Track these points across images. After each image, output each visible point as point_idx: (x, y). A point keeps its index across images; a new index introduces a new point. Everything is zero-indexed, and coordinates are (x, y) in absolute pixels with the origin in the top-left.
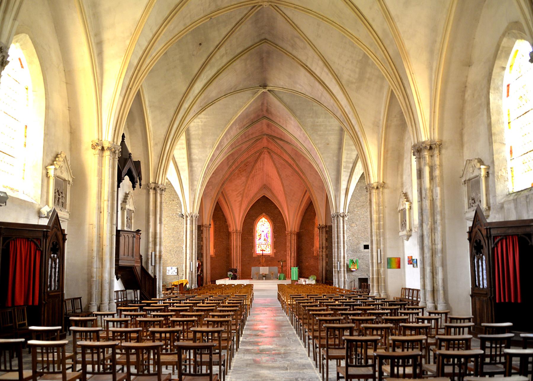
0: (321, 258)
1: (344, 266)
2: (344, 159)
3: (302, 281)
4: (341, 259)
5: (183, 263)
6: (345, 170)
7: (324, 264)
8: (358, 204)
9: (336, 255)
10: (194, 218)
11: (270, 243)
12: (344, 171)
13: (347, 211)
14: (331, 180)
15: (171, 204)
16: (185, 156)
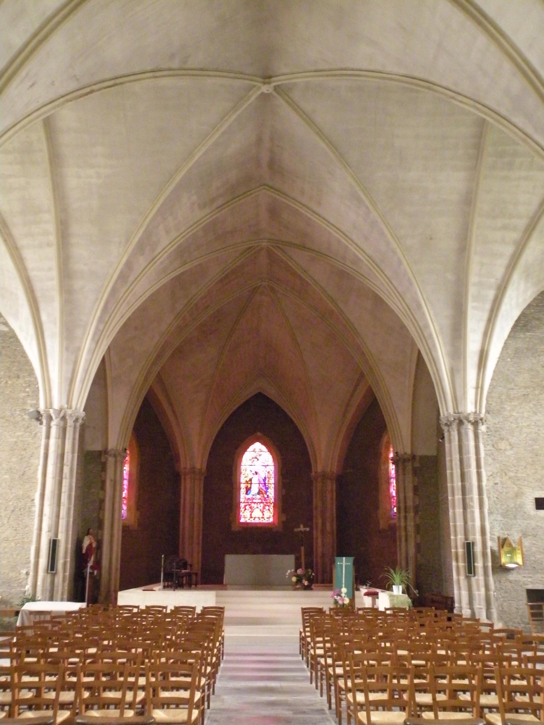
1: (484, 555)
2: (473, 279)
4: (474, 534)
5: (30, 542)
6: (475, 304)
7: (412, 551)
8: (512, 393)
10: (70, 422)
11: (272, 500)
12: (474, 308)
13: (484, 411)
16: (53, 264)
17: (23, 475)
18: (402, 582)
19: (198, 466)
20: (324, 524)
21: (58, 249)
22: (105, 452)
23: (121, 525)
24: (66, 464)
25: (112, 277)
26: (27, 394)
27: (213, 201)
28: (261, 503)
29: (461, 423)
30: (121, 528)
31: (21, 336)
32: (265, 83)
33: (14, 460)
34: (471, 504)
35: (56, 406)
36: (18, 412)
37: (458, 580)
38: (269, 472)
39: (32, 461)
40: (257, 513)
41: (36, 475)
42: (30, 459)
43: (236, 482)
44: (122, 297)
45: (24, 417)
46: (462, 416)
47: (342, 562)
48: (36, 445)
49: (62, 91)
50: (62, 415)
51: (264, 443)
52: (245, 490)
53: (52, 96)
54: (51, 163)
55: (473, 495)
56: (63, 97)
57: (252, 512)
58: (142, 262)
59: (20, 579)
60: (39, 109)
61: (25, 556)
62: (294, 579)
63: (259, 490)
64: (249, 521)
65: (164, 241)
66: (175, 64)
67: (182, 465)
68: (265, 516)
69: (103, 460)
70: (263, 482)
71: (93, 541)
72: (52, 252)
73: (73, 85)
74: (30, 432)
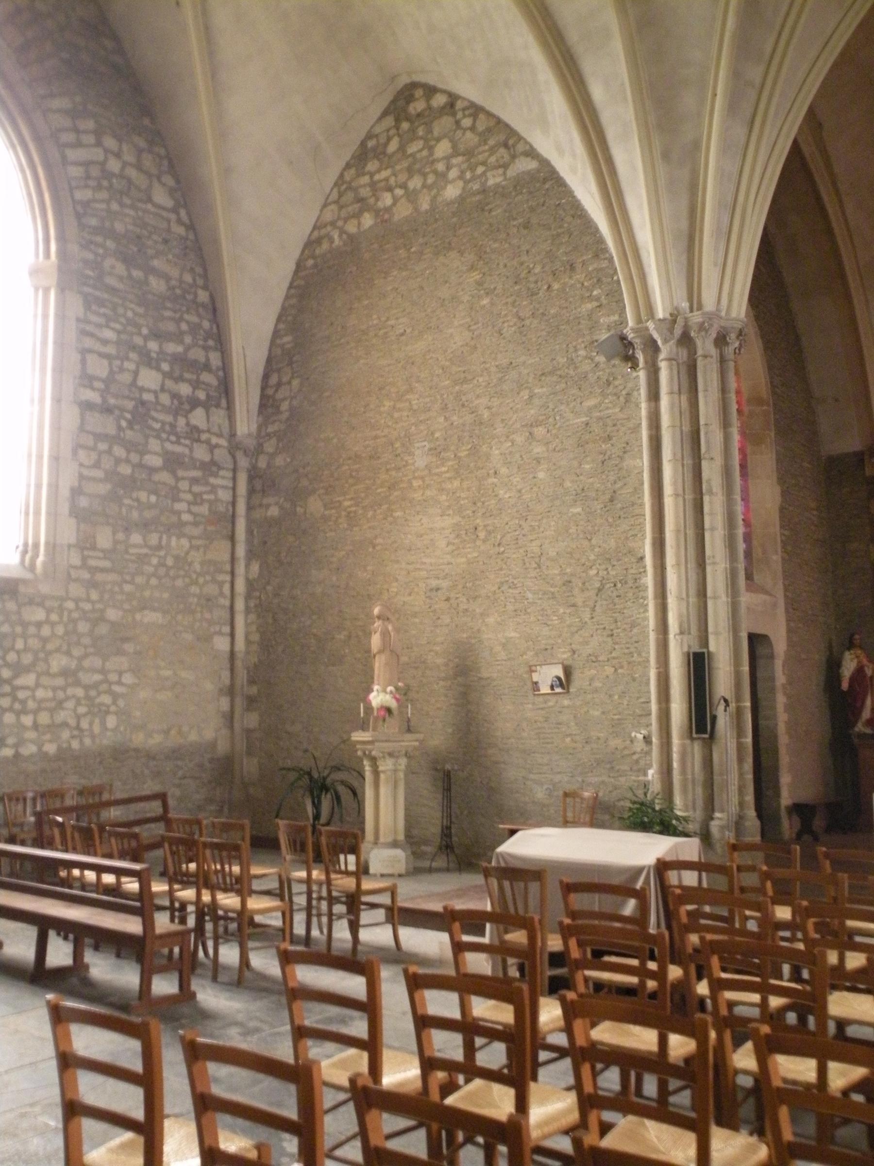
10: (705, 345)
24: (707, 456)
26: (595, 304)
36: (582, 353)
41: (641, 497)
42: (621, 458)
45: (597, 359)
48: (631, 425)
50: (678, 331)
59: (634, 753)
61: (638, 698)
71: (865, 661)
74: (615, 394)
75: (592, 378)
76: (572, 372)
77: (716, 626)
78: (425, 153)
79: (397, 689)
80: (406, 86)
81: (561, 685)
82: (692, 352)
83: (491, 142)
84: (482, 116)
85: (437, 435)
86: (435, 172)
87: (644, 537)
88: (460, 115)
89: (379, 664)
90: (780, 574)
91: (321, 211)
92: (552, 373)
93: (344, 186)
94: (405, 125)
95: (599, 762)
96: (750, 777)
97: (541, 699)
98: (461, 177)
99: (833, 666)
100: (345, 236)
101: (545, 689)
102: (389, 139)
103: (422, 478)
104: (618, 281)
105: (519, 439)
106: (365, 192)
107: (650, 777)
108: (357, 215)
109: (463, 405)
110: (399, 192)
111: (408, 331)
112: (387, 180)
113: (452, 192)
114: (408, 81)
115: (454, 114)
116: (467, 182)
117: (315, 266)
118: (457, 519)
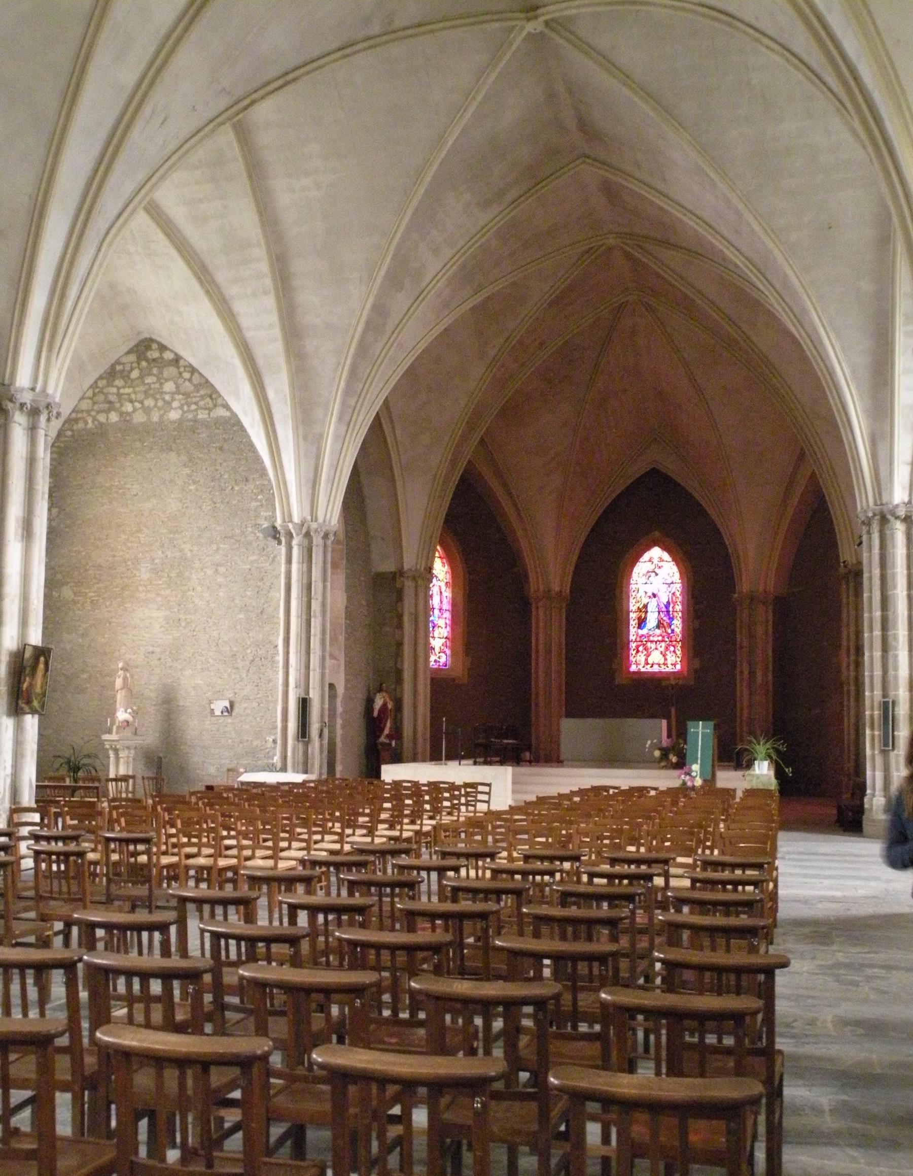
0: (852, 688)
3: (727, 779)
9: (878, 673)
10: (317, 540)
14: (853, 372)
15: (240, 492)
17: (261, 613)
18: (769, 757)
19: (556, 588)
20: (752, 673)
21: (278, 297)
22: (401, 573)
23: (429, 676)
25: (356, 329)
26: (259, 503)
27: (501, 194)
28: (663, 641)
29: (884, 520)
30: (429, 681)
31: (246, 422)
32: (528, 19)
33: (249, 593)
34: (894, 643)
35: (296, 519)
36: (250, 529)
37: (873, 756)
38: (674, 594)
39: (272, 594)
40: (656, 657)
41: (278, 614)
43: (622, 610)
44: (379, 356)
46: (885, 508)
47: (698, 728)
49: (210, 114)
50: (304, 531)
51: (665, 548)
52: (636, 621)
53: (195, 124)
54: (250, 177)
55: (897, 630)
56: (211, 121)
57: (648, 655)
58: (401, 301)
60: (181, 146)
62: (657, 753)
63: (659, 622)
64: (643, 670)
65: (433, 265)
66: (376, 29)
67: (533, 587)
68: (669, 662)
69: (398, 585)
70: (664, 609)
71: (388, 700)
72: (270, 302)
73: (225, 101)
74: (266, 555)
75: (255, 544)
76: (243, 540)
77: (314, 684)
78: (157, 386)
79: (133, 711)
80: (146, 339)
81: (228, 711)
82: (311, 542)
83: (202, 392)
84: (196, 375)
85: (157, 561)
86: (163, 399)
87: (278, 635)
88: (182, 369)
89: (120, 696)
90: (343, 647)
91: (79, 401)
92: (232, 537)
93: (97, 390)
94: (144, 364)
95: (247, 753)
96: (325, 761)
97: (215, 719)
98: (181, 408)
99: (370, 702)
100: (96, 423)
101: (218, 713)
102: (132, 369)
103: (145, 586)
104: (273, 494)
105: (210, 572)
106: (113, 398)
107: (275, 761)
108: (107, 411)
109: (175, 546)
110: (137, 405)
111: (140, 494)
112: (129, 394)
113: (174, 415)
114: (148, 336)
115: (178, 368)
116: (184, 412)
117: (73, 436)
118: (168, 613)
